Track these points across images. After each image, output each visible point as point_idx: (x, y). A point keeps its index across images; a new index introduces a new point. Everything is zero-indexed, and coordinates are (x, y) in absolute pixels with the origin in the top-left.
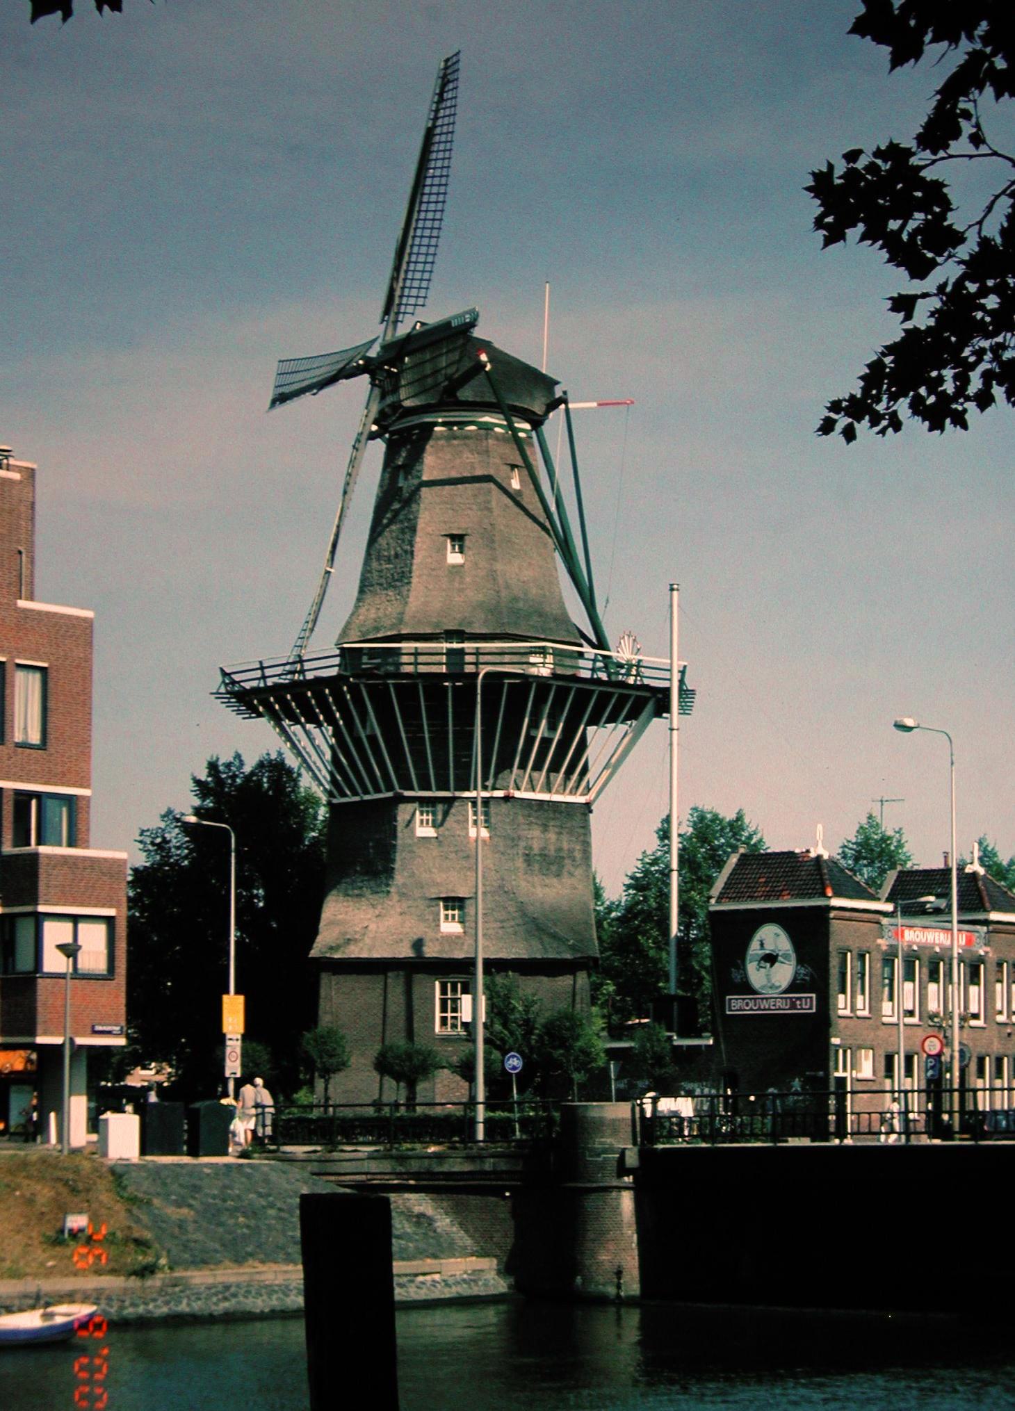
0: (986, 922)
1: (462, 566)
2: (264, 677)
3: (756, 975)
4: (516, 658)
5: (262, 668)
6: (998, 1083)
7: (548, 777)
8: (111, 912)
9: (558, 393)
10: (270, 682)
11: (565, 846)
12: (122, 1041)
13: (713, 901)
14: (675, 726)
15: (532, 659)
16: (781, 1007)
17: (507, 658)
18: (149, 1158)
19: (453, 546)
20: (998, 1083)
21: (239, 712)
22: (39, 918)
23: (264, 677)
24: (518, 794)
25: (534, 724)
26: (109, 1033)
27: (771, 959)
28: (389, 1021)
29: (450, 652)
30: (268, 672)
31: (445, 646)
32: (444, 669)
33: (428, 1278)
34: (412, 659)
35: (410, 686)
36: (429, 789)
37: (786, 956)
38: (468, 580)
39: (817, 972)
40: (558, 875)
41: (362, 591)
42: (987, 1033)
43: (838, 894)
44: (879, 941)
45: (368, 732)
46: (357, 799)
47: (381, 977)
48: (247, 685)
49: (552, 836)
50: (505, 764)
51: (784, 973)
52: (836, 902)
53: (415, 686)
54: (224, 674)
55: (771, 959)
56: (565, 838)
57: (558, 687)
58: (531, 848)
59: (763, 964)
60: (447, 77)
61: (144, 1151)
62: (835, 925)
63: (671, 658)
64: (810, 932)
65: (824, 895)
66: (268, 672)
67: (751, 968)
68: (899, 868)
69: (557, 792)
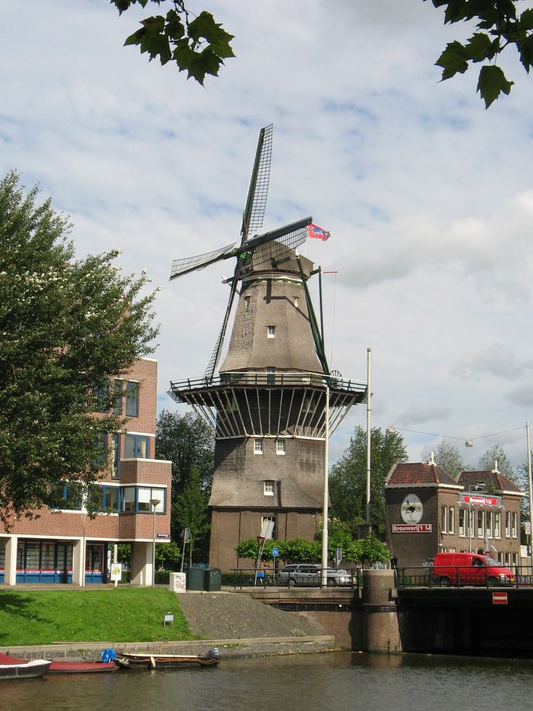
0: (501, 495)
1: (274, 339)
2: (189, 385)
3: (406, 516)
4: (296, 379)
5: (189, 382)
6: (506, 564)
7: (304, 427)
8: (165, 486)
9: (315, 268)
10: (192, 388)
11: (317, 459)
12: (169, 541)
13: (386, 484)
14: (369, 409)
15: (304, 379)
16: (418, 528)
17: (293, 379)
18: (191, 592)
19: (270, 331)
20: (506, 564)
21: (175, 400)
22: (136, 488)
23: (189, 385)
24: (297, 437)
25: (305, 407)
26: (164, 537)
27: (412, 509)
28: (241, 534)
29: (269, 376)
30: (191, 383)
31: (267, 373)
32: (266, 383)
33: (308, 643)
34: (280, 379)
35: (252, 391)
36: (238, 435)
37: (419, 508)
38: (276, 345)
39: (431, 516)
40: (314, 471)
41: (230, 350)
42: (502, 542)
43: (441, 482)
44: (459, 502)
45: (304, 411)
46: (228, 438)
47: (239, 513)
48: (180, 389)
49: (311, 455)
50: (292, 423)
51: (418, 515)
52: (441, 485)
53: (280, 391)
54: (172, 384)
55: (412, 509)
56: (316, 456)
57: (308, 390)
58: (303, 460)
59: (408, 511)
60: (263, 131)
61: (188, 588)
62: (440, 495)
63: (368, 380)
64: (428, 495)
65: (436, 482)
66: (191, 383)
67: (403, 513)
68: (462, 471)
69: (307, 436)
